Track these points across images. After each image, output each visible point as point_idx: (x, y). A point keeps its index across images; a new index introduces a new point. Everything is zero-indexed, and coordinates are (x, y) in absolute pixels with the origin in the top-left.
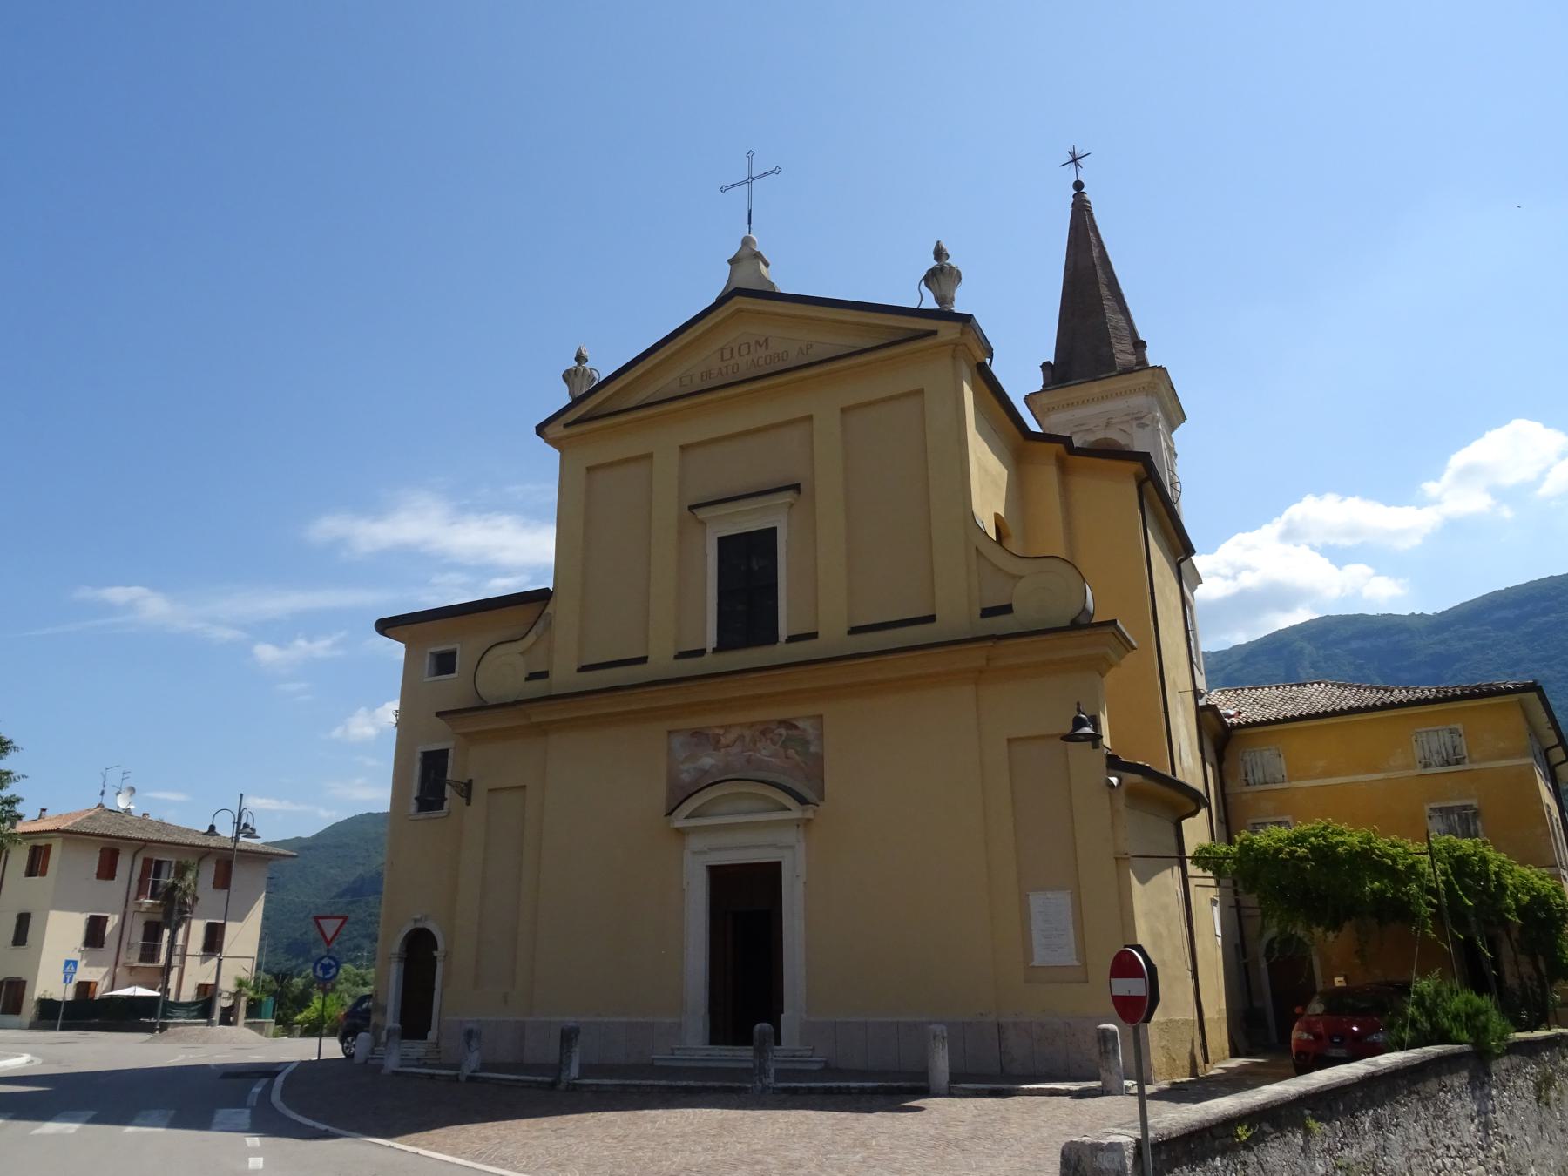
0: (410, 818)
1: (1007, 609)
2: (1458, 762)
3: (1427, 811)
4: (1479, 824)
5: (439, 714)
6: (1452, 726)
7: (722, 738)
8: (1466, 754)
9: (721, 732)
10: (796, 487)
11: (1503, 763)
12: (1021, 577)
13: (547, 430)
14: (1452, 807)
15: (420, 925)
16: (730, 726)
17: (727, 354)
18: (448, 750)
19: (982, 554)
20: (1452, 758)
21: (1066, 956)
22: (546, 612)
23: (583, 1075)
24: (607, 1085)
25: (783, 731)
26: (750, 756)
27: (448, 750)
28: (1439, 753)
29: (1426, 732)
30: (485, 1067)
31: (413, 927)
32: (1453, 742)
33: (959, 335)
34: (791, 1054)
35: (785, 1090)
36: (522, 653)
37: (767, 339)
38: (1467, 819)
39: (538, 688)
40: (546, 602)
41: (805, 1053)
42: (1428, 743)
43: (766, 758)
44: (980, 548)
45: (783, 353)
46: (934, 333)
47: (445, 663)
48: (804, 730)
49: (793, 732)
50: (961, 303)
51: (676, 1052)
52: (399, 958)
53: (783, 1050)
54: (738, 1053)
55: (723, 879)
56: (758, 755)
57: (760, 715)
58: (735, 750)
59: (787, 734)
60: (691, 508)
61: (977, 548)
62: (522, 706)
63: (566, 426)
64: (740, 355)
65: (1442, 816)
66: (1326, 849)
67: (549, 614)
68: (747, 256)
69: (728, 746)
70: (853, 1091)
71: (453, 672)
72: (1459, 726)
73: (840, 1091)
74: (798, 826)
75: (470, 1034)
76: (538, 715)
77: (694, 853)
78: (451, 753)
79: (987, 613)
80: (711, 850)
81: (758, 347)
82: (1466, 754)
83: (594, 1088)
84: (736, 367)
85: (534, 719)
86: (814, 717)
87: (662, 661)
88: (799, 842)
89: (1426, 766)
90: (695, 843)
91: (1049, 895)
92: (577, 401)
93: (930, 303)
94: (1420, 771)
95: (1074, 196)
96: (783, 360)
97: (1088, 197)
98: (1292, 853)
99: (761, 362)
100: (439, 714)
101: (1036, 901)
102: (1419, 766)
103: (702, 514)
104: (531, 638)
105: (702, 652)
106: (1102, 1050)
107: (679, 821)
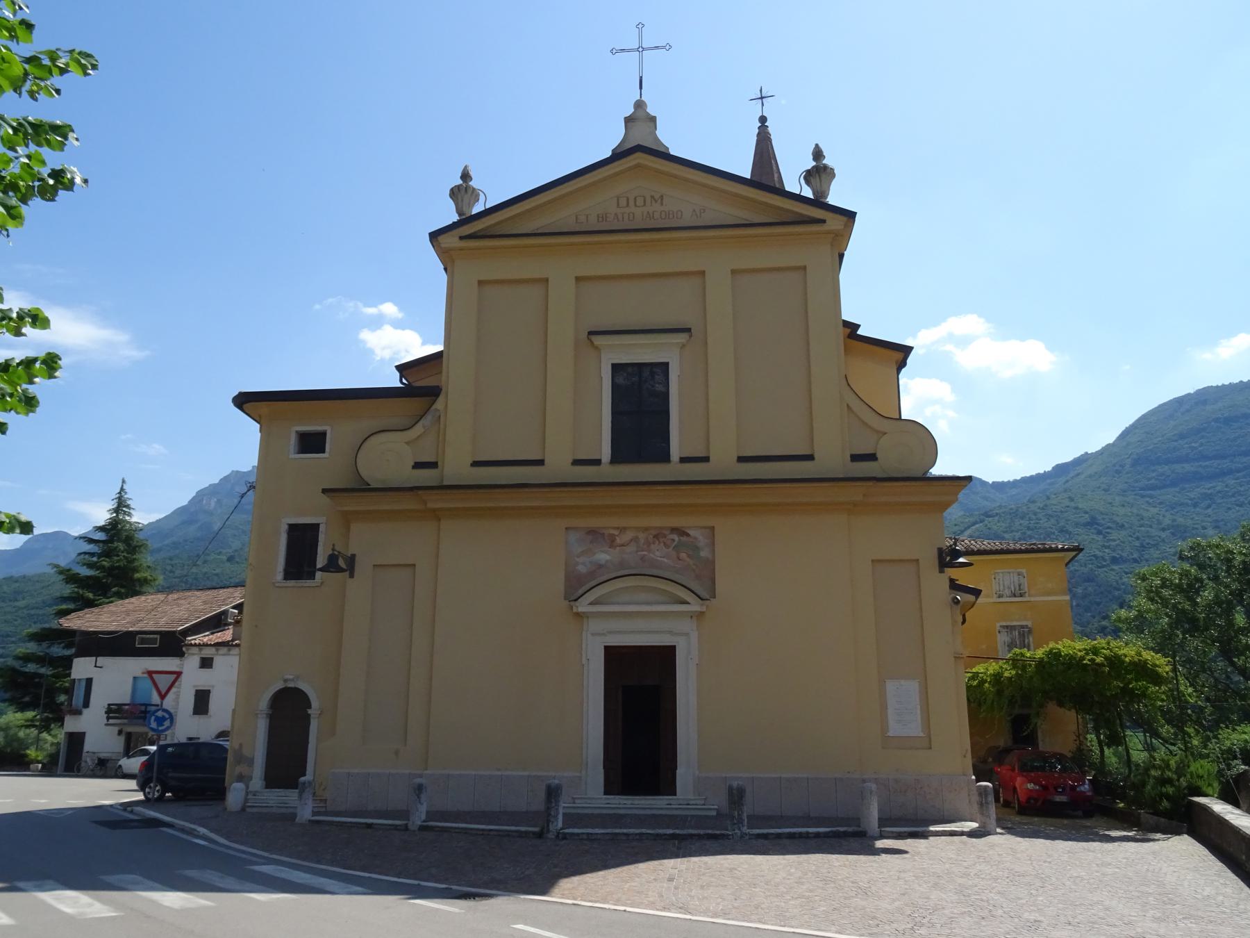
0: (277, 585)
1: (872, 457)
2: (1021, 596)
3: (998, 628)
4: (1031, 639)
5: (324, 491)
6: (1019, 570)
7: (617, 538)
8: (1026, 590)
9: (616, 532)
10: (688, 330)
11: (1050, 598)
12: (885, 433)
13: (441, 238)
14: (1014, 626)
15: (291, 685)
16: (625, 528)
17: (623, 202)
18: (318, 525)
19: (852, 411)
20: (1018, 592)
21: (914, 729)
22: (434, 407)
23: (565, 826)
24: (597, 834)
25: (676, 537)
26: (644, 555)
27: (318, 525)
28: (1009, 588)
29: (1002, 573)
30: (431, 815)
31: (284, 686)
32: (1019, 581)
33: (843, 227)
34: (686, 802)
35: (759, 836)
36: (407, 443)
37: (662, 196)
38: (1024, 635)
39: (426, 477)
40: (434, 398)
41: (698, 802)
42: (1003, 580)
43: (659, 558)
44: (850, 405)
45: (677, 212)
46: (824, 221)
47: (312, 443)
48: (696, 538)
49: (684, 539)
50: (835, 198)
51: (577, 801)
52: (267, 714)
53: (678, 799)
54: (636, 802)
55: (616, 657)
56: (652, 555)
57: (656, 521)
58: (632, 548)
59: (680, 540)
60: (590, 333)
61: (848, 405)
62: (420, 492)
63: (461, 238)
64: (636, 205)
65: (1007, 632)
66: (1113, 659)
67: (437, 410)
68: (640, 118)
69: (623, 545)
70: (810, 835)
71: (323, 451)
72: (1024, 571)
73: (801, 835)
74: (691, 617)
75: (420, 789)
76: (436, 502)
77: (593, 634)
78: (322, 528)
79: (855, 458)
80: (610, 632)
81: (653, 202)
82: (1026, 590)
83: (638, 837)
84: (680, 213)
85: (430, 505)
86: (705, 528)
87: (558, 464)
88: (692, 630)
89: (1000, 596)
90: (594, 625)
91: (903, 682)
92: (465, 220)
93: (808, 192)
94: (995, 599)
95: (759, 128)
96: (677, 218)
97: (770, 130)
98: (1092, 660)
99: (657, 215)
100: (324, 491)
101: (891, 686)
102: (995, 596)
103: (598, 340)
104: (418, 429)
105: (597, 462)
106: (984, 802)
107: (582, 606)
